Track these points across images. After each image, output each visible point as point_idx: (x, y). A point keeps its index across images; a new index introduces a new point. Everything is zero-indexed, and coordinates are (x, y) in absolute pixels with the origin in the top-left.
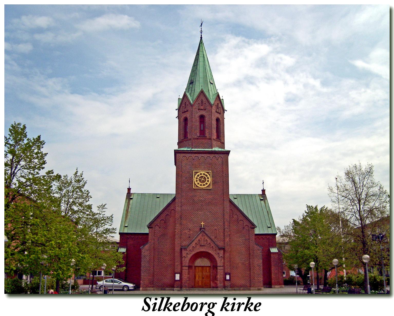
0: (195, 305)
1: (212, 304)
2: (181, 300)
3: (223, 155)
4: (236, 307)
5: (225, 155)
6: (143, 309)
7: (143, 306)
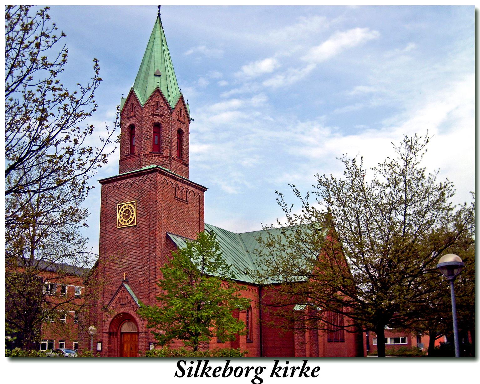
0: (240, 370)
1: (259, 369)
2: (223, 364)
4: (289, 372)
6: (176, 374)
7: (177, 371)
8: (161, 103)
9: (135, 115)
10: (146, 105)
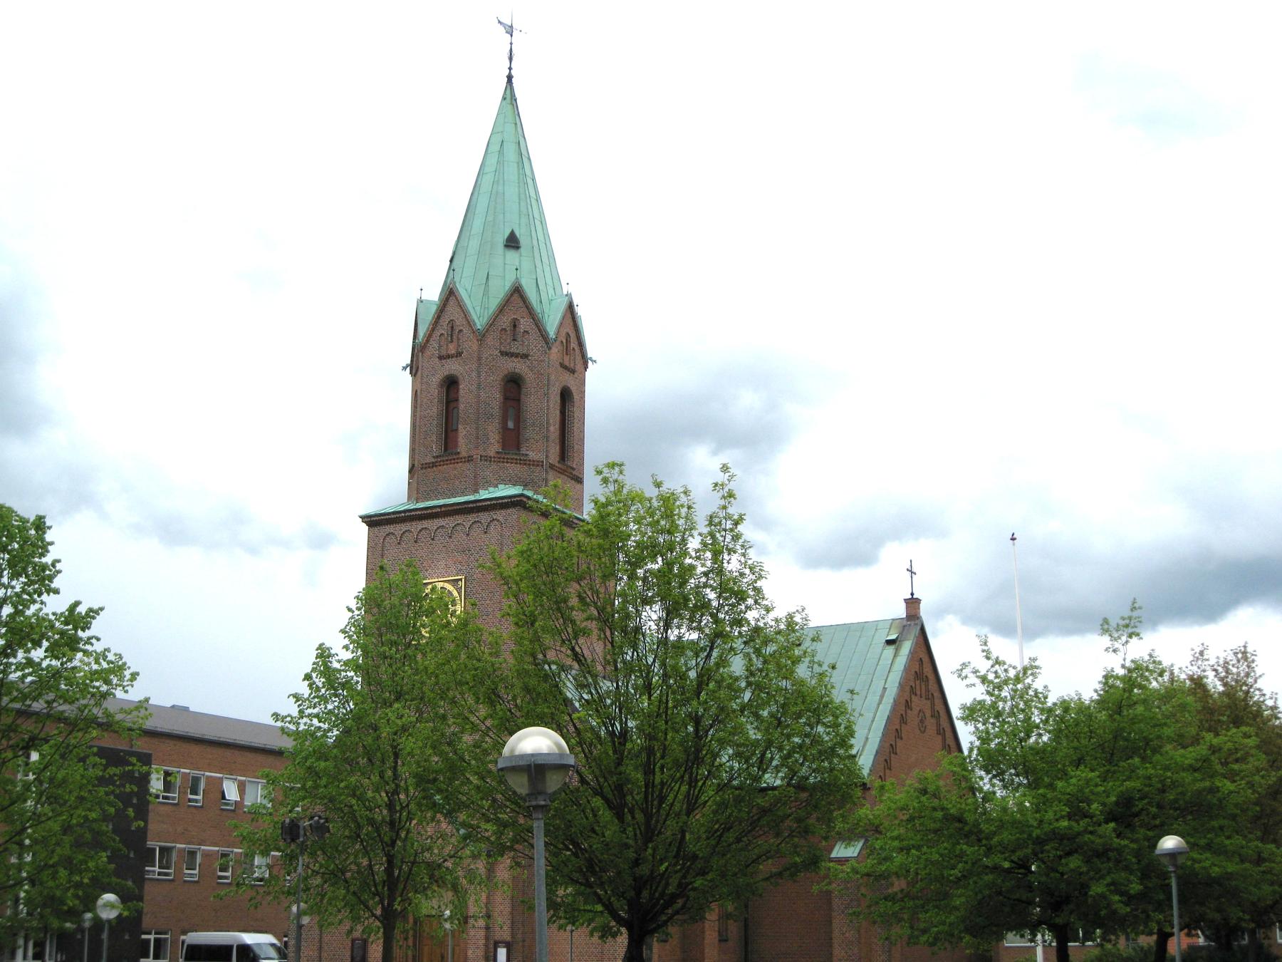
3: (503, 512)
5: (509, 511)
8: (525, 324)
9: (459, 354)
10: (488, 329)
